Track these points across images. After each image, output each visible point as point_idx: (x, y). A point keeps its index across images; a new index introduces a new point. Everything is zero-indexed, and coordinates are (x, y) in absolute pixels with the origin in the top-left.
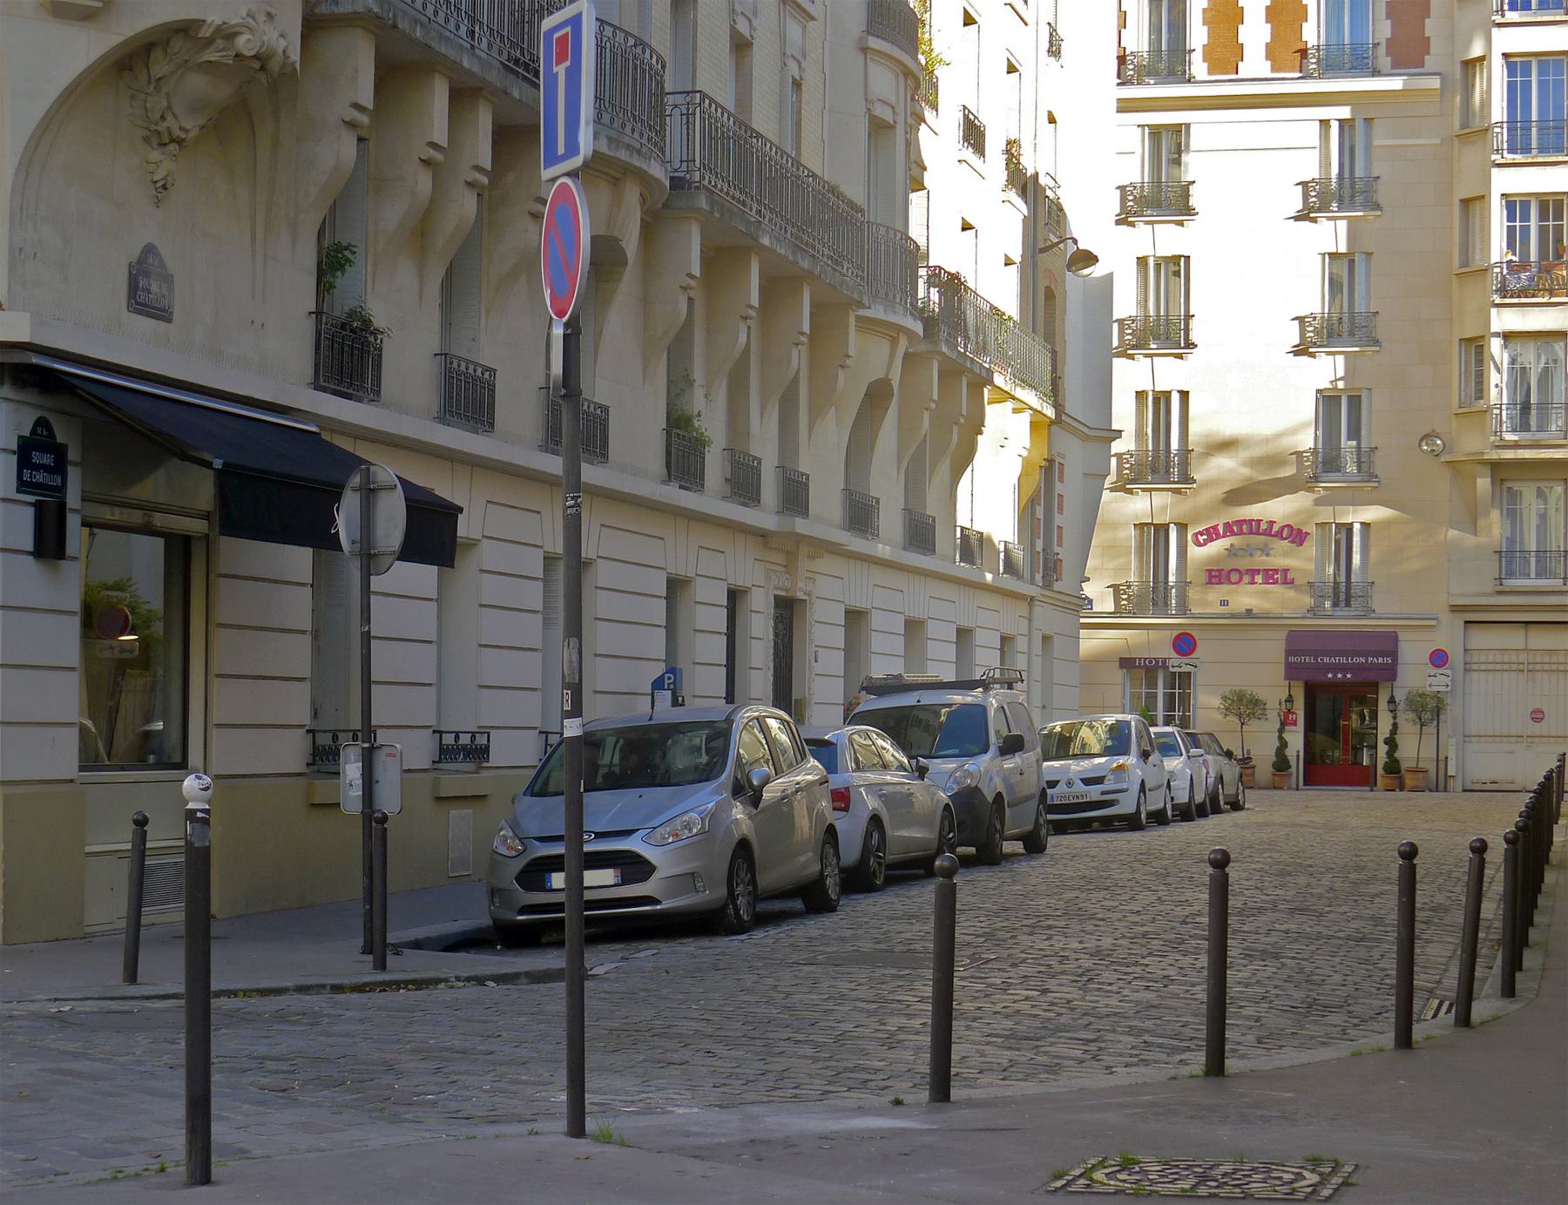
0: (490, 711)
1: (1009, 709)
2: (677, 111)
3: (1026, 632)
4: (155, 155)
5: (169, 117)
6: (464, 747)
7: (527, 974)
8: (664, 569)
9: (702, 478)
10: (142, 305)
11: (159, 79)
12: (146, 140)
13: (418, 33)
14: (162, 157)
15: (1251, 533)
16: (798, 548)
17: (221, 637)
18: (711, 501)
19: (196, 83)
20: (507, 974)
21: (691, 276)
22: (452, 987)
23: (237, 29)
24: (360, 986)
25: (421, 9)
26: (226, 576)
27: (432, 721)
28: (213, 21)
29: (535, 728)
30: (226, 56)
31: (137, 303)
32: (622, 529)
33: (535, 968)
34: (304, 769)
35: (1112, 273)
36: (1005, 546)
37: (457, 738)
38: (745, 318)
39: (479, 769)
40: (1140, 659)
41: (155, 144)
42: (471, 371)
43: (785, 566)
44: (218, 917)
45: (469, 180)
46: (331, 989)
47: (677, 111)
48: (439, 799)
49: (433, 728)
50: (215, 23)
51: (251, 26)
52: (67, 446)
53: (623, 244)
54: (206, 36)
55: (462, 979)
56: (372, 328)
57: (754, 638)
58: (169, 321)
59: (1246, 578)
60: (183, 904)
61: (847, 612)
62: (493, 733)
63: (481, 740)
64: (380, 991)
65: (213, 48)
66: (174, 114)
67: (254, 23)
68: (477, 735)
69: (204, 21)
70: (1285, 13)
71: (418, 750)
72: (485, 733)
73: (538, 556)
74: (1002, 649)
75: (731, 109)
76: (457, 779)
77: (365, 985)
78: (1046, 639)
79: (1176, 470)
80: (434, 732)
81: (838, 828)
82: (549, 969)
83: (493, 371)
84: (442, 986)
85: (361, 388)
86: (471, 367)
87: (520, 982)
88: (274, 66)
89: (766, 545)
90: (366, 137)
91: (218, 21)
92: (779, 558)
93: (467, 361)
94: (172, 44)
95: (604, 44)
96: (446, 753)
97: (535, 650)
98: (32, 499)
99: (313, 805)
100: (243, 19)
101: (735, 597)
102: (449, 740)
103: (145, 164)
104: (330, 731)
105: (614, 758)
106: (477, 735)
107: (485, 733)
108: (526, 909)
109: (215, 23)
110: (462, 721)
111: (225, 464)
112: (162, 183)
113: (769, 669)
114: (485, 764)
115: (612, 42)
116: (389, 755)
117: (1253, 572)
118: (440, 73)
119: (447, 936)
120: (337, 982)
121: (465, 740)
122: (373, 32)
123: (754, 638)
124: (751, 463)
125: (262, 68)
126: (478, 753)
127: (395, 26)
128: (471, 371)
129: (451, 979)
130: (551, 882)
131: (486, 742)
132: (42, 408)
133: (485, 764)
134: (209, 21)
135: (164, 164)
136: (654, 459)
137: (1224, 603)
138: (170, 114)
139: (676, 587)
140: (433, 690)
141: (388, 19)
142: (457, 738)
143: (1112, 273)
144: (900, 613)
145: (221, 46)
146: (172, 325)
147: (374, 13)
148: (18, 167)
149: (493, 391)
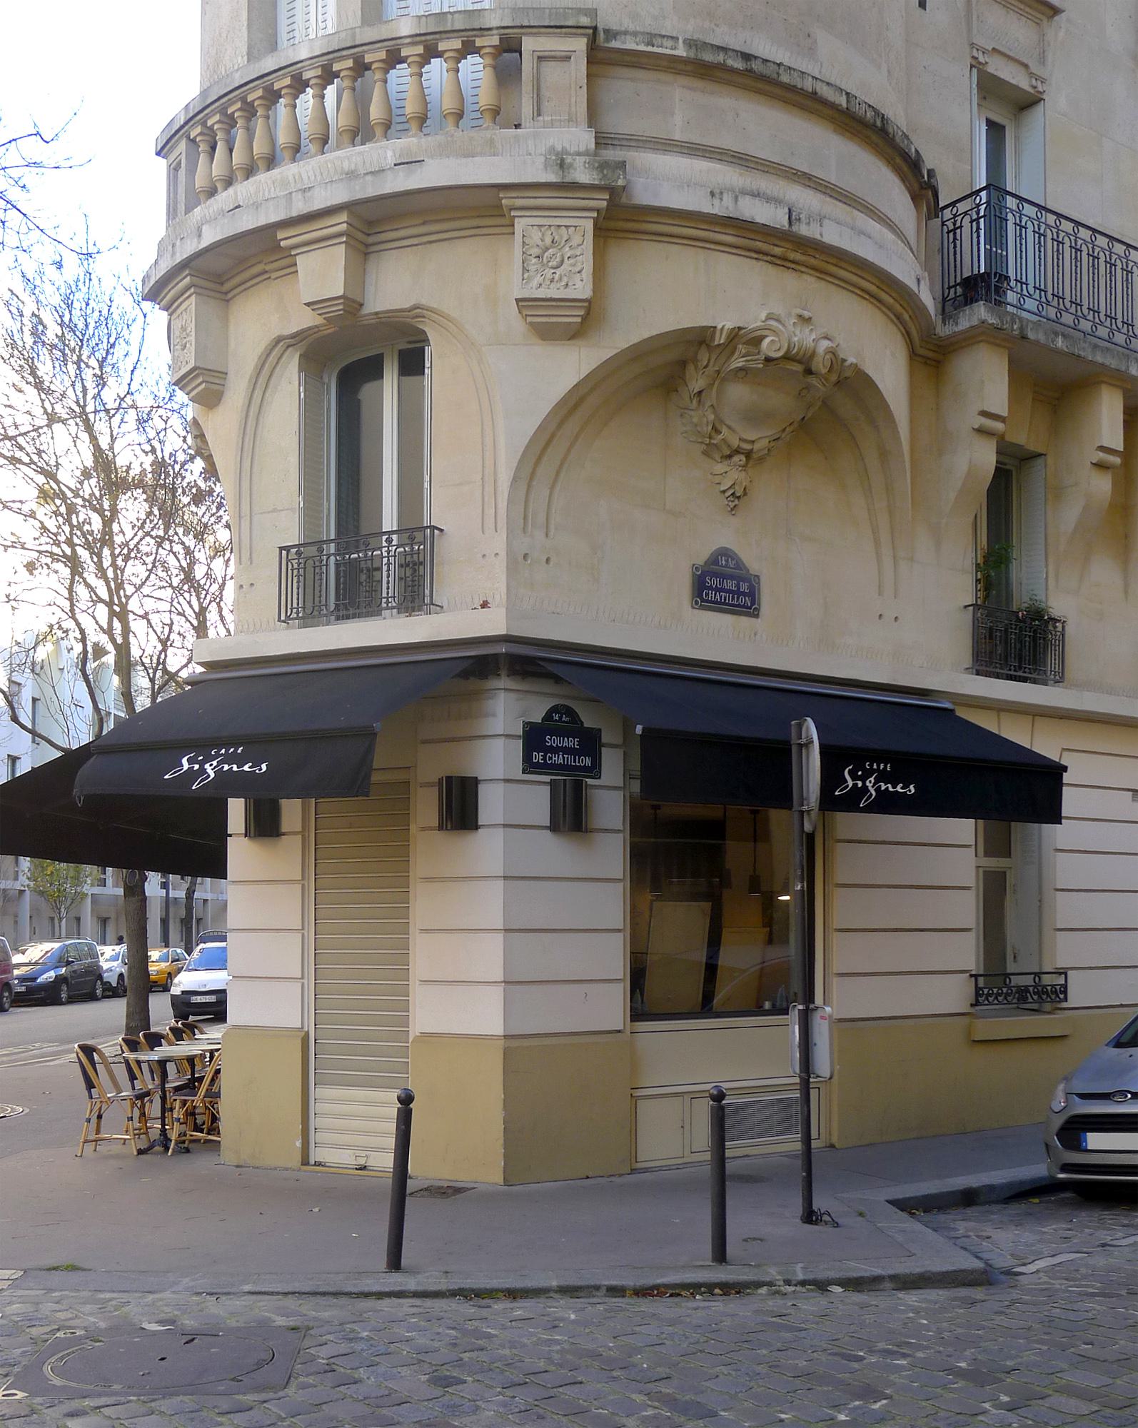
1: (1055, 1018)
2: (967, 219)
4: (720, 468)
5: (724, 430)
7: (893, 1277)
10: (711, 602)
11: (700, 392)
12: (705, 453)
13: (1060, 343)
14: (727, 469)
17: (838, 893)
19: (738, 393)
20: (862, 1277)
22: (777, 1292)
23: (759, 333)
24: (647, 1289)
25: (1125, 345)
28: (723, 326)
30: (752, 360)
33: (907, 1271)
34: (967, 1009)
41: (717, 457)
44: (837, 1147)
45: (976, 427)
46: (607, 1291)
47: (967, 219)
50: (726, 327)
51: (773, 328)
52: (600, 730)
54: (722, 342)
55: (794, 1282)
56: (1046, 618)
60: (799, 1135)
64: (671, 1295)
65: (736, 356)
66: (729, 427)
67: (780, 327)
69: (715, 327)
77: (657, 1287)
82: (926, 1272)
84: (764, 1290)
87: (881, 1287)
88: (820, 365)
90: (1040, 450)
91: (729, 325)
94: (699, 357)
95: (1129, 269)
98: (547, 778)
99: (974, 1041)
100: (763, 322)
103: (710, 476)
108: (1066, 1168)
109: (726, 327)
111: (644, 729)
114: (1064, 1005)
115: (1124, 261)
116: (823, 1018)
118: (1105, 383)
119: (1021, 1183)
120: (614, 1283)
122: (1004, 347)
125: (809, 372)
127: (1024, 337)
129: (778, 1283)
130: (1086, 1142)
132: (552, 695)
133: (1064, 1005)
134: (719, 327)
135: (731, 474)
138: (724, 426)
141: (1013, 330)
145: (743, 351)
146: (759, 620)
147: (990, 324)
148: (514, 479)
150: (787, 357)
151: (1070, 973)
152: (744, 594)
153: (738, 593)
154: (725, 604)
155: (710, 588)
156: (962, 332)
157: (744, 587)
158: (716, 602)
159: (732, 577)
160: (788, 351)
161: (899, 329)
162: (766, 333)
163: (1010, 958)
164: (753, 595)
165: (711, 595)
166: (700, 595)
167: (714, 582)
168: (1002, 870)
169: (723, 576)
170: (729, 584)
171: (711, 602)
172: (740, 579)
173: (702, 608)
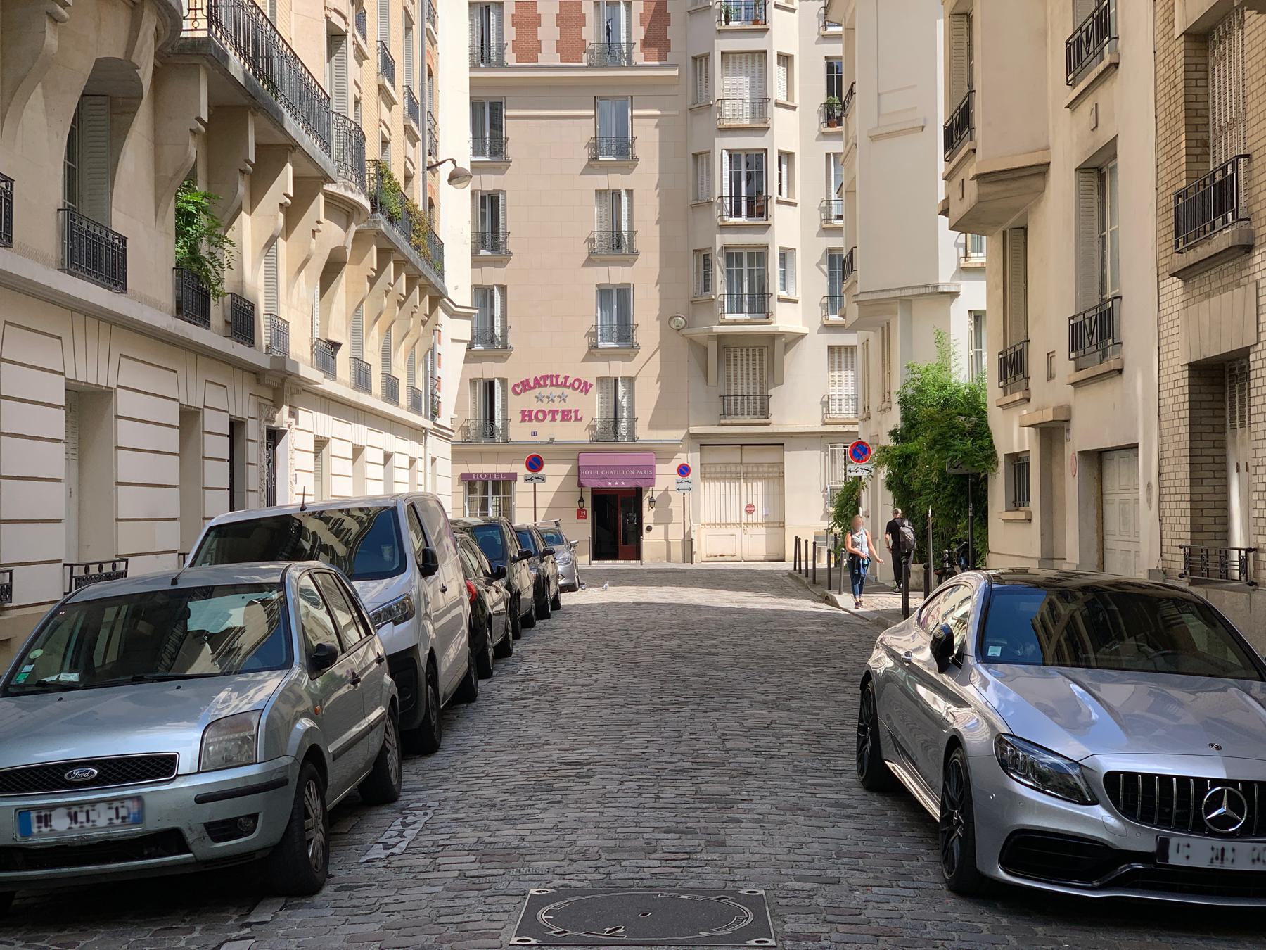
3: (423, 456)
8: (178, 400)
15: (552, 385)
16: (283, 384)
18: (213, 337)
21: (199, 120)
26: (7, 434)
29: (59, 561)
32: (153, 365)
36: (232, 299)
37: (101, 568)
40: (476, 474)
42: (104, 235)
43: (272, 401)
49: (64, 562)
53: (139, 72)
57: (251, 464)
59: (549, 417)
61: (232, 424)
62: (15, 569)
68: (117, 563)
70: (570, 20)
72: (7, 571)
73: (381, 453)
74: (231, 436)
78: (433, 460)
79: (367, 176)
80: (179, 554)
86: (98, 229)
89: (258, 381)
92: (269, 394)
93: (95, 223)
97: (175, 486)
102: (80, 572)
104: (110, 562)
105: (1207, 450)
106: (117, 563)
107: (7, 571)
113: (263, 491)
114: (8, 605)
117: (554, 412)
121: (107, 568)
123: (251, 464)
124: (110, 239)
128: (104, 235)
131: (8, 581)
133: (8, 605)
137: (534, 434)
142: (101, 568)
144: (174, 399)
149: (11, 203)
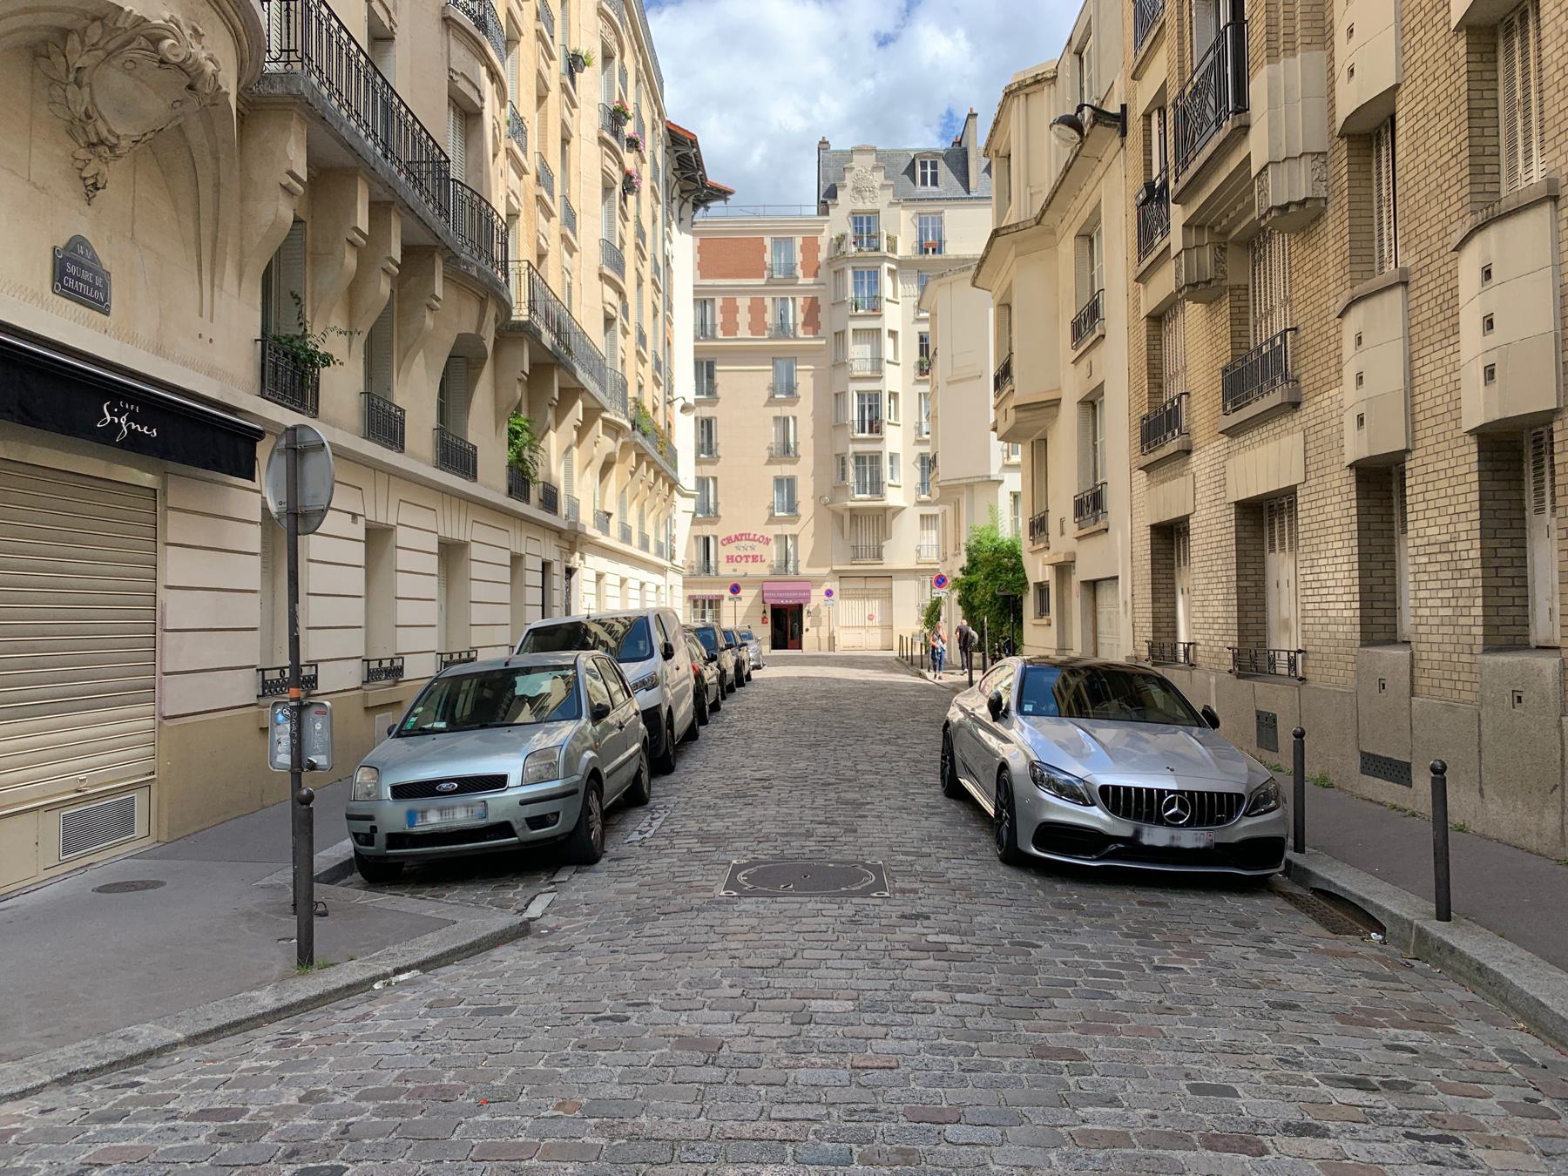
0: (405, 641)
6: (386, 669)
9: (403, 441)
10: (70, 289)
14: (91, 157)
23: (160, 31)
27: (361, 653)
31: (63, 287)
34: (254, 701)
35: (766, 524)
37: (380, 663)
38: (551, 405)
39: (397, 683)
45: (284, 183)
48: (367, 709)
58: (107, 314)
63: (398, 663)
71: (351, 675)
74: (543, 572)
75: (365, 49)
76: (381, 692)
81: (1365, 453)
83: (402, 410)
85: (305, 407)
96: (372, 676)
101: (546, 566)
102: (374, 665)
110: (383, 652)
112: (92, 181)
114: (314, 692)
117: (747, 557)
121: (386, 664)
126: (395, 672)
133: (314, 692)
136: (502, 483)
139: (516, 560)
140: (363, 630)
142: (380, 663)
143: (766, 524)
150: (180, 67)
151: (319, 665)
152: (98, 288)
153: (92, 285)
154: (81, 294)
155: (70, 275)
156: (276, 96)
157: (98, 282)
158: (74, 291)
159: (90, 270)
160: (184, 61)
161: (1188, 408)
162: (169, 34)
163: (889, 653)
164: (105, 288)
165: (71, 282)
166: (61, 281)
167: (72, 269)
168: (796, 602)
169: (82, 266)
170: (87, 276)
171: (70, 289)
172: (96, 273)
173: (61, 295)
